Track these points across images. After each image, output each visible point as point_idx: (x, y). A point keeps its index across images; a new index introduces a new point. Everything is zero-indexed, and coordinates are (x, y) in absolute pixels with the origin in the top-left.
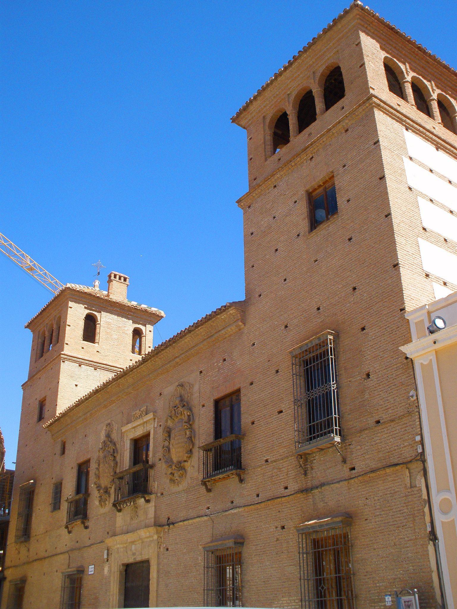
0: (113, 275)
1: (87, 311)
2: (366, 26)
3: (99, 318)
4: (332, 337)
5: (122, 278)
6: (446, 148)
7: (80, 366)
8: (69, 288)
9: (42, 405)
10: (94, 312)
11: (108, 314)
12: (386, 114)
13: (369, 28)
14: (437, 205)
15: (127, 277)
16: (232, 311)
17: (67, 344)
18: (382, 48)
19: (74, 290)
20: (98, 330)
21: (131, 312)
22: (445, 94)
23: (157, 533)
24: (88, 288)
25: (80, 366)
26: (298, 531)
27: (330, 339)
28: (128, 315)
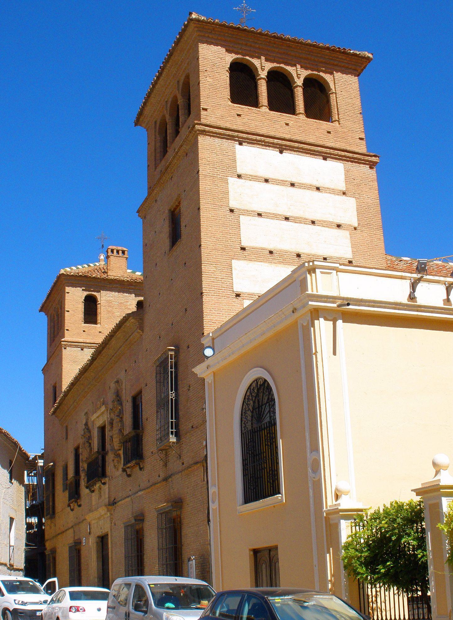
0: (109, 251)
1: (86, 293)
2: (207, 35)
3: (98, 298)
4: (173, 353)
5: (120, 252)
6: (294, 147)
7: (82, 350)
8: (63, 274)
9: (55, 388)
10: (93, 293)
11: (108, 292)
12: (213, 136)
13: (210, 36)
14: (268, 217)
15: (125, 249)
16: (132, 320)
17: (68, 330)
18: (228, 51)
19: (68, 275)
20: (99, 311)
21: (132, 285)
22: (317, 73)
23: (108, 510)
24: (89, 266)
25: (82, 350)
26: (157, 511)
27: (171, 355)
28: (129, 289)
